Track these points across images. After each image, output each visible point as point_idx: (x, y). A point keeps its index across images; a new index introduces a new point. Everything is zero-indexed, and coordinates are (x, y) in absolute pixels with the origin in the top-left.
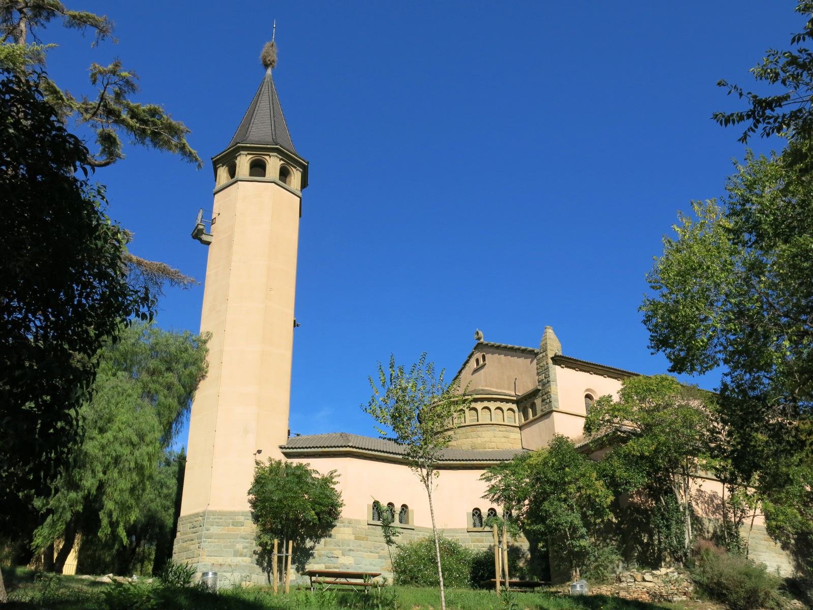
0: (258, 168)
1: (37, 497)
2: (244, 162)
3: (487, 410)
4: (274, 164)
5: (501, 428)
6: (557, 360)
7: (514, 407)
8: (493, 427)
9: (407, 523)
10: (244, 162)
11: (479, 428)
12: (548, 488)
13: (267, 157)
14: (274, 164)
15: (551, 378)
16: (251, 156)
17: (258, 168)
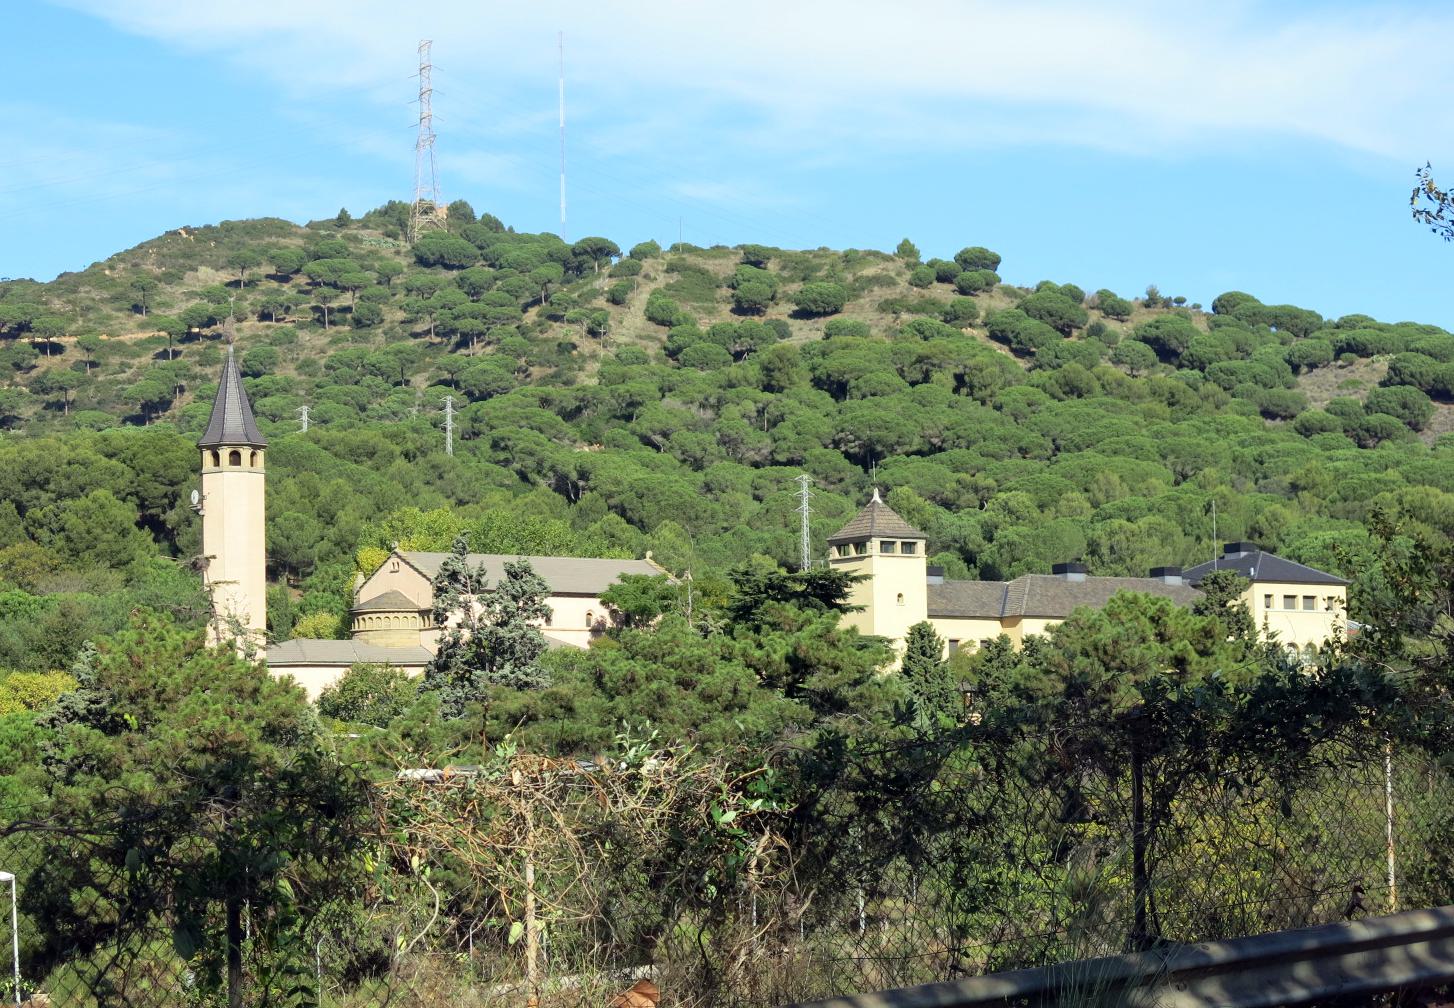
0: (235, 458)
2: (225, 453)
4: (245, 453)
7: (417, 615)
10: (225, 453)
17: (235, 458)
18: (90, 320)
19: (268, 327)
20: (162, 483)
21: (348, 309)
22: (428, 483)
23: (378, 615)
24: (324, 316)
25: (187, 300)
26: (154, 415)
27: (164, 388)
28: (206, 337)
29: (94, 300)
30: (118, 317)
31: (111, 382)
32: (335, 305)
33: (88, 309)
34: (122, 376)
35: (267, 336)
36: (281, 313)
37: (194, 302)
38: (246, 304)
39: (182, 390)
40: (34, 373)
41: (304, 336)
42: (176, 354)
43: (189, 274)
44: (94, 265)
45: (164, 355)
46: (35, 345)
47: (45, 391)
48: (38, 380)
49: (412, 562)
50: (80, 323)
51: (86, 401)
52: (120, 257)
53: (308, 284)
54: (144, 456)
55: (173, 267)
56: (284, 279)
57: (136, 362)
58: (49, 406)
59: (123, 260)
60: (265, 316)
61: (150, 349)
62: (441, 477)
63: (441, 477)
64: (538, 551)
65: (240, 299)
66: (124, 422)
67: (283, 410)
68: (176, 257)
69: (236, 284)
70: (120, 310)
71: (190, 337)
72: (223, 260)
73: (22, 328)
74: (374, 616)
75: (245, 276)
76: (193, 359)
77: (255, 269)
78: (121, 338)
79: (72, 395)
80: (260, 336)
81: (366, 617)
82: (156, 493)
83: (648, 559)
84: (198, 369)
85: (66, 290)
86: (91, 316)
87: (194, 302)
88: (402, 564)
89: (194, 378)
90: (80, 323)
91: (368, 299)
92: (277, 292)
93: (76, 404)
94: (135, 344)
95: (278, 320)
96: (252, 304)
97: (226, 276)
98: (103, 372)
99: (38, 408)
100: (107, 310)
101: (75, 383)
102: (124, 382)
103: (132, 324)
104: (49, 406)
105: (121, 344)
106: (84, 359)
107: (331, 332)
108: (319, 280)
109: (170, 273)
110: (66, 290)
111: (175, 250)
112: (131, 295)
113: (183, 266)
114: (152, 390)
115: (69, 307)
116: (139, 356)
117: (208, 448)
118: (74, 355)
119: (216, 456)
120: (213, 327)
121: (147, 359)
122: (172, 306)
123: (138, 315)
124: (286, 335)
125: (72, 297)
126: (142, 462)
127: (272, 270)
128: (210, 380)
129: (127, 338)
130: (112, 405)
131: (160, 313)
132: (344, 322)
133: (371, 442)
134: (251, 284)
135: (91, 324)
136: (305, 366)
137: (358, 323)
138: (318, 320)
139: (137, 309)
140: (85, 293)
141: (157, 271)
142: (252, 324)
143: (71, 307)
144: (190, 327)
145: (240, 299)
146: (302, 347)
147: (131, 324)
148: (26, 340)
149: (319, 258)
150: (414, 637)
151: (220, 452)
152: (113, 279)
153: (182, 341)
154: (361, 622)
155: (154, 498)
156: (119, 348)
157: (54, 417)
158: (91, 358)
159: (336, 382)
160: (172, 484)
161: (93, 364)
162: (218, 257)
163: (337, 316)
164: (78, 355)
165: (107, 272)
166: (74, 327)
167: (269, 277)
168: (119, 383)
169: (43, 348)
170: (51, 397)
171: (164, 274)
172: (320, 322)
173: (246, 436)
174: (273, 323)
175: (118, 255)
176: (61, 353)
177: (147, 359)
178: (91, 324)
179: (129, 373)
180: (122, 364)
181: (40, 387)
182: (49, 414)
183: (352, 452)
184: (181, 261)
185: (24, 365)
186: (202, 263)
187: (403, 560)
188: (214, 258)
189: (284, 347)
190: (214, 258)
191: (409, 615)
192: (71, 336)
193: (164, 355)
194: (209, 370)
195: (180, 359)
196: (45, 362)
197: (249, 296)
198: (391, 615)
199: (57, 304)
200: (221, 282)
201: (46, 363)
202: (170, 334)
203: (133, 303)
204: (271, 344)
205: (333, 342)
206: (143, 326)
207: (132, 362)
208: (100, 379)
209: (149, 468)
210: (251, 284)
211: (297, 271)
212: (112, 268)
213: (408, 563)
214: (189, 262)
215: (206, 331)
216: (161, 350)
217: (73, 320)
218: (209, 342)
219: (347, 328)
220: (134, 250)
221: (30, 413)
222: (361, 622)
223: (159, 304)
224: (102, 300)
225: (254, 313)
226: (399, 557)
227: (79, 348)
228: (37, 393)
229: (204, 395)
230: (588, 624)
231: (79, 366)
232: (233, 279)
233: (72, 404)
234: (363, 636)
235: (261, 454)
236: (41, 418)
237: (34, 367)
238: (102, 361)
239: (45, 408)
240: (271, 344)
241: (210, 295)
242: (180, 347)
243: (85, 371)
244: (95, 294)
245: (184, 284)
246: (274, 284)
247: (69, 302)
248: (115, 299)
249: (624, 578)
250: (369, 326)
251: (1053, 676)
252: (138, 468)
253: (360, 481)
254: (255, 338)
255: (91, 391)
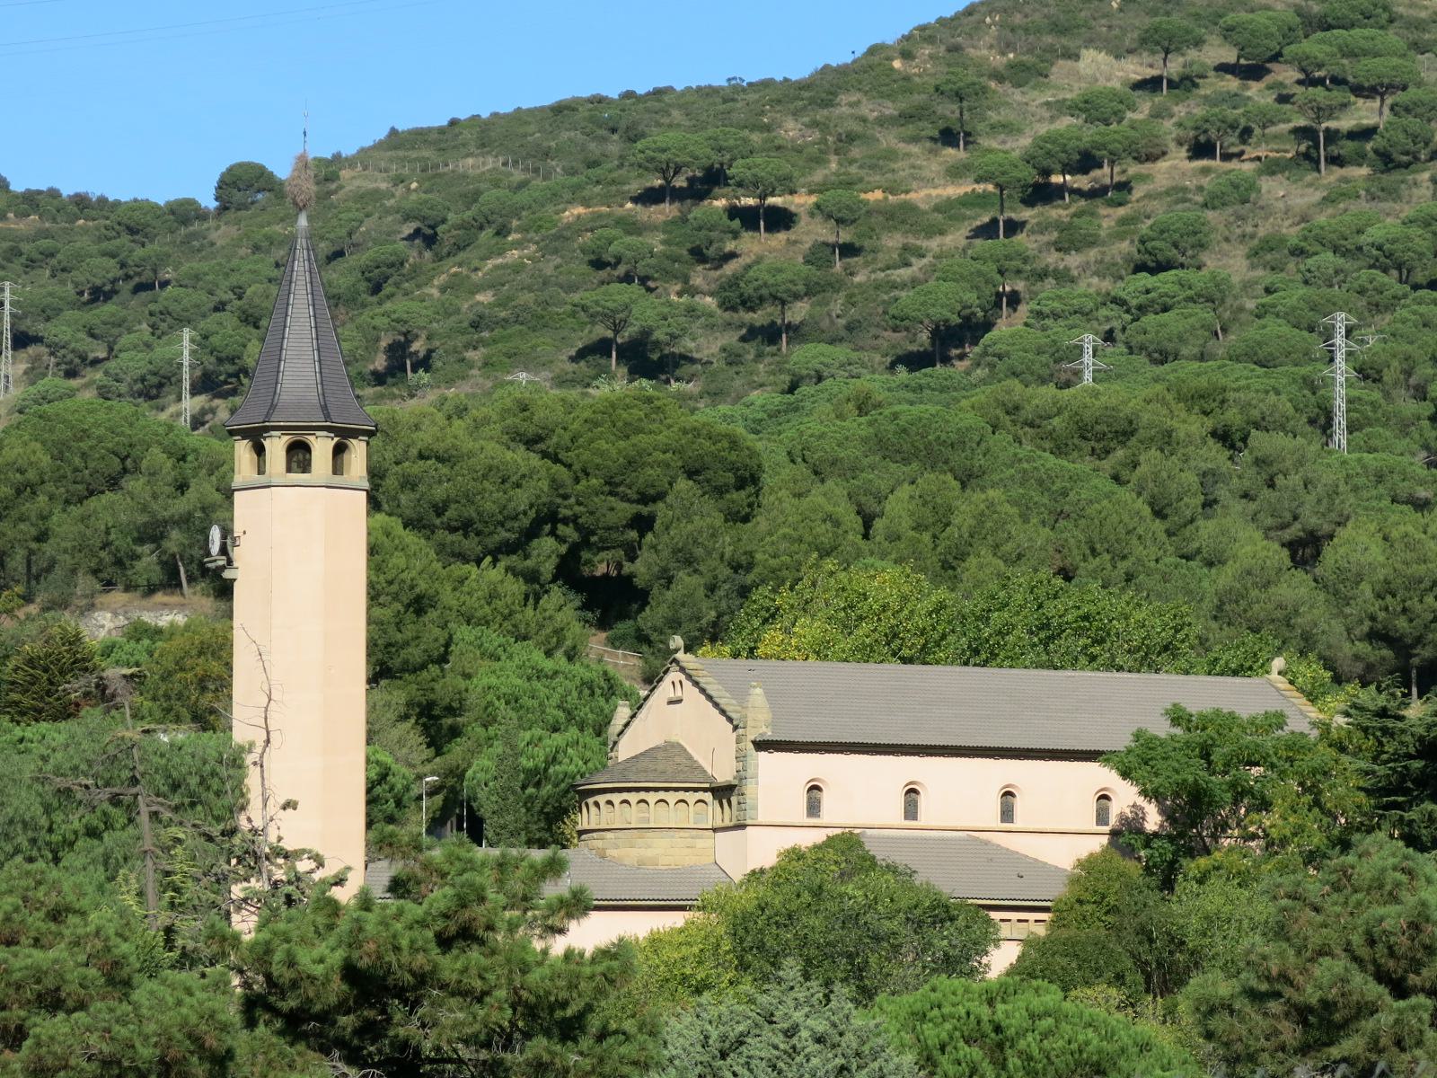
0: (299, 455)
1: (246, 995)
2: (276, 446)
3: (643, 804)
4: (322, 447)
5: (682, 833)
6: (761, 745)
7: (708, 796)
8: (671, 833)
9: (915, 818)
10: (276, 446)
11: (650, 834)
12: (1261, 834)
13: (312, 438)
14: (322, 447)
15: (750, 772)
16: (287, 438)
17: (299, 455)
18: (851, 162)
19: (1205, 171)
20: (625, 499)
21: (1366, 133)
22: (1245, 496)
23: (625, 796)
24: (1317, 147)
25: (1053, 119)
26: (955, 352)
27: (971, 297)
28: (1078, 193)
29: (864, 120)
30: (908, 155)
31: (878, 287)
32: (1345, 123)
33: (851, 138)
34: (903, 274)
35: (1200, 189)
36: (1231, 142)
37: (1065, 122)
38: (1168, 124)
39: (1014, 300)
40: (730, 268)
41: (1274, 188)
42: (1013, 227)
43: (1062, 66)
44: (873, 50)
45: (988, 231)
46: (733, 212)
47: (748, 304)
48: (734, 282)
49: (711, 690)
50: (834, 166)
51: (825, 324)
52: (925, 34)
53: (1300, 82)
54: (592, 441)
55: (1030, 51)
56: (1253, 72)
57: (934, 244)
58: (752, 333)
59: (930, 40)
60: (1201, 150)
61: (964, 218)
62: (1271, 484)
63: (1271, 484)
64: (1093, 658)
65: (1157, 114)
66: (892, 367)
67: (1181, 339)
68: (1038, 31)
69: (1152, 84)
70: (915, 139)
71: (1042, 194)
72: (1129, 40)
73: (713, 179)
74: (616, 798)
75: (1175, 67)
76: (1045, 238)
77: (1192, 54)
78: (912, 196)
79: (798, 312)
80: (1185, 190)
81: (602, 799)
82: (612, 519)
83: (1274, 676)
84: (1052, 259)
85: (812, 101)
86: (856, 152)
87: (1065, 122)
88: (688, 684)
89: (1042, 275)
90: (834, 166)
91: (1407, 110)
92: (1234, 99)
93: (805, 329)
94: (937, 209)
95: (1227, 157)
96: (1180, 125)
97: (1136, 68)
98: (867, 264)
99: (731, 338)
100: (888, 139)
101: (801, 288)
102: (903, 286)
103: (935, 167)
104: (752, 333)
105: (910, 208)
106: (832, 239)
107: (1332, 178)
108: (1321, 73)
109: (1022, 64)
110: (812, 101)
111: (1037, 17)
112: (940, 110)
113: (1051, 49)
114: (949, 299)
115: (816, 135)
116: (942, 232)
117: (245, 434)
118: (813, 232)
119: (259, 450)
120: (1096, 173)
121: (956, 238)
122: (1020, 131)
123: (951, 151)
124: (1236, 187)
125: (821, 114)
126: (586, 456)
127: (1230, 56)
128: (1073, 280)
129: (921, 196)
130: (873, 331)
131: (995, 145)
132: (1359, 159)
133: (1127, 411)
134: (1185, 83)
135: (853, 169)
136: (1263, 251)
137: (1387, 161)
138: (1306, 156)
139: (948, 137)
140: (852, 107)
141: (997, 60)
142: (1176, 166)
143: (817, 135)
144: (1046, 173)
145: (1157, 114)
146: (1267, 211)
147: (934, 167)
148: (720, 203)
149: (1329, 27)
150: (700, 843)
151: (267, 443)
152: (907, 78)
153: (1029, 202)
154: (593, 809)
155: (609, 529)
156: (901, 217)
157: (759, 356)
158: (845, 236)
159: (1306, 282)
160: (644, 499)
161: (848, 250)
162: (1124, 30)
163: (1348, 147)
164: (823, 232)
165: (897, 64)
166: (818, 176)
167: (1223, 68)
168: (894, 286)
169: (749, 219)
170: (759, 317)
171: (1011, 66)
172: (1310, 159)
173: (324, 408)
174: (1216, 163)
175: (922, 28)
176: (788, 228)
177: (956, 238)
178: (853, 169)
179: (918, 264)
180: (905, 248)
181: (737, 298)
182: (750, 350)
183: (1084, 431)
184: (1049, 39)
185: (711, 252)
186: (1089, 43)
187: (689, 677)
188: (1117, 32)
189: (1230, 210)
190: (1117, 32)
191: (691, 797)
192: (811, 192)
193: (988, 231)
194: (1073, 261)
195: (1020, 238)
196: (755, 246)
197: (1176, 109)
198: (652, 797)
199: (791, 130)
200: (1125, 82)
201: (756, 248)
202: (1001, 187)
203: (942, 124)
204: (1205, 205)
205: (1328, 200)
206: (955, 173)
207: (925, 244)
208: (857, 279)
209: (598, 467)
210: (1185, 83)
211: (1276, 57)
212: (907, 55)
213: (696, 684)
214: (1064, 41)
215: (1082, 182)
216: (986, 219)
217: (819, 160)
218: (1083, 203)
219: (1364, 171)
220: (956, 17)
221: (715, 349)
222: (593, 809)
223: (993, 127)
224: (882, 122)
225: (1180, 143)
226: (682, 670)
227: (819, 219)
228: (733, 309)
229: (1046, 310)
230: (1102, 818)
231: (820, 255)
232: (1150, 73)
233: (796, 332)
234: (595, 842)
235: (358, 452)
236: (733, 359)
237: (732, 255)
238: (867, 243)
239: (743, 339)
240: (1205, 205)
241: (1088, 107)
242: (1026, 214)
243: (830, 264)
244: (869, 110)
245: (1048, 86)
246: (1232, 83)
247: (814, 124)
248: (906, 117)
249: (1178, 717)
250: (1407, 166)
251: (1275, 1006)
252: (576, 467)
253: (1065, 494)
254: (1177, 194)
255: (837, 305)
